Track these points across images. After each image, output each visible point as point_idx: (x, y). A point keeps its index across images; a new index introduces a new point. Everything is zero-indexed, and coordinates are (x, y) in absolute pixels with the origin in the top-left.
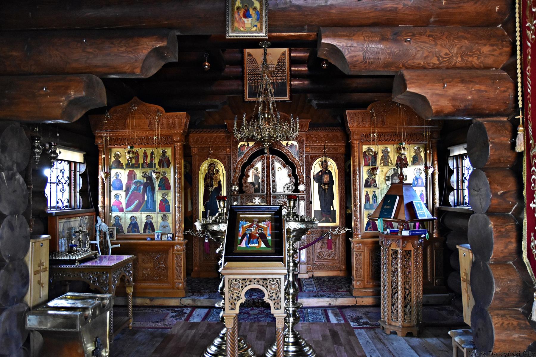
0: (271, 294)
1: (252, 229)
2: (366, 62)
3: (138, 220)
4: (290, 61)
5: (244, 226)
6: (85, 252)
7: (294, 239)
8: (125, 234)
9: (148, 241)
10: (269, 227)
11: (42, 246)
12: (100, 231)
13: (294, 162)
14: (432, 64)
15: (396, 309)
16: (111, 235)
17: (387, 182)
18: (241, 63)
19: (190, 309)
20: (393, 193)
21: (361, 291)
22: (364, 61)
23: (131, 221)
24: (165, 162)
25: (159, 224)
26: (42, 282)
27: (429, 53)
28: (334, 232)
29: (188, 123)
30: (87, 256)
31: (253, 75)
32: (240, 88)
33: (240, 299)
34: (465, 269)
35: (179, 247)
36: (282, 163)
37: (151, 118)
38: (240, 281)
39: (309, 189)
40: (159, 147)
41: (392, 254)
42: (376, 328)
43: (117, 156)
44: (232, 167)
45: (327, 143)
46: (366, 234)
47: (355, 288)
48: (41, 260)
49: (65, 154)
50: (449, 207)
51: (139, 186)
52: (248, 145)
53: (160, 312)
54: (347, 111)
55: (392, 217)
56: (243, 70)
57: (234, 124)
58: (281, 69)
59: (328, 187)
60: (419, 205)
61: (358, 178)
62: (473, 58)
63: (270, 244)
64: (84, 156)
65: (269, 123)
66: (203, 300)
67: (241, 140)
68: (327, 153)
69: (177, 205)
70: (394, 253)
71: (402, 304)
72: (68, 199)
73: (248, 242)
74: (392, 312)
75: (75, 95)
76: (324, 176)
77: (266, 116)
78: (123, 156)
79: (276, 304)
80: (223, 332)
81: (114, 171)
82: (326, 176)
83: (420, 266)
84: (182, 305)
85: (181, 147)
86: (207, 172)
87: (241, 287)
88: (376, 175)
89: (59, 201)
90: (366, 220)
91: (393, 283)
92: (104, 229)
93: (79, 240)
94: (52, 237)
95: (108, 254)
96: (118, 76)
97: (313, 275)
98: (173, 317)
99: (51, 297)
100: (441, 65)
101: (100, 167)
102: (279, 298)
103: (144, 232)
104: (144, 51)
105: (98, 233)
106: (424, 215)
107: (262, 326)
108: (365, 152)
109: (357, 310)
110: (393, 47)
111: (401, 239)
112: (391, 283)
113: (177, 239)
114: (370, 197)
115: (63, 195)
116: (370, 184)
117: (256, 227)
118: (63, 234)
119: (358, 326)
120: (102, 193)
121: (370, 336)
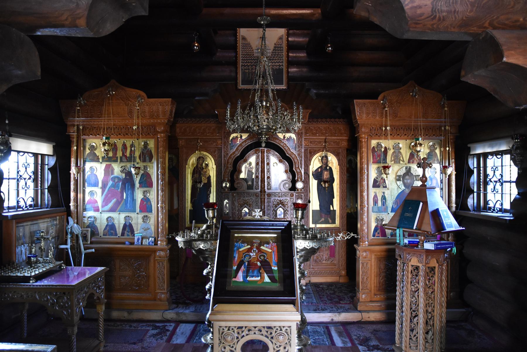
0: (277, 347)
1: (251, 254)
2: (436, 16)
3: (116, 222)
4: (287, 46)
5: (241, 250)
8: (100, 236)
9: (127, 246)
10: (274, 251)
12: (72, 233)
13: (291, 157)
15: (415, 336)
16: (85, 238)
17: (398, 182)
18: (234, 47)
19: (173, 325)
20: (415, 198)
21: (367, 305)
23: (108, 222)
24: (146, 156)
25: (139, 226)
29: (174, 111)
30: (47, 269)
32: (233, 74)
35: (162, 253)
36: (278, 158)
37: (131, 105)
38: (236, 330)
39: (307, 187)
41: (411, 271)
44: (223, 161)
46: (374, 240)
47: (360, 301)
51: (118, 182)
52: (241, 137)
53: (139, 328)
54: (355, 101)
55: (415, 228)
56: (237, 54)
57: (226, 113)
58: (278, 55)
59: (329, 185)
60: (445, 213)
61: (366, 177)
63: (276, 275)
64: (54, 147)
65: (267, 113)
66: (188, 313)
67: (234, 131)
68: (328, 148)
69: (159, 205)
72: (33, 197)
73: (247, 274)
74: (410, 339)
77: (264, 104)
82: (326, 173)
83: (443, 285)
84: (164, 319)
85: (165, 138)
86: (195, 166)
87: (236, 338)
88: (389, 174)
90: (373, 225)
91: (412, 305)
92: (76, 231)
93: (40, 248)
98: (154, 336)
103: (123, 234)
105: (69, 236)
106: (451, 227)
108: (374, 147)
109: (363, 327)
111: (424, 254)
112: (411, 304)
113: (160, 244)
115: (26, 192)
116: (379, 184)
117: (257, 251)
120: (74, 190)
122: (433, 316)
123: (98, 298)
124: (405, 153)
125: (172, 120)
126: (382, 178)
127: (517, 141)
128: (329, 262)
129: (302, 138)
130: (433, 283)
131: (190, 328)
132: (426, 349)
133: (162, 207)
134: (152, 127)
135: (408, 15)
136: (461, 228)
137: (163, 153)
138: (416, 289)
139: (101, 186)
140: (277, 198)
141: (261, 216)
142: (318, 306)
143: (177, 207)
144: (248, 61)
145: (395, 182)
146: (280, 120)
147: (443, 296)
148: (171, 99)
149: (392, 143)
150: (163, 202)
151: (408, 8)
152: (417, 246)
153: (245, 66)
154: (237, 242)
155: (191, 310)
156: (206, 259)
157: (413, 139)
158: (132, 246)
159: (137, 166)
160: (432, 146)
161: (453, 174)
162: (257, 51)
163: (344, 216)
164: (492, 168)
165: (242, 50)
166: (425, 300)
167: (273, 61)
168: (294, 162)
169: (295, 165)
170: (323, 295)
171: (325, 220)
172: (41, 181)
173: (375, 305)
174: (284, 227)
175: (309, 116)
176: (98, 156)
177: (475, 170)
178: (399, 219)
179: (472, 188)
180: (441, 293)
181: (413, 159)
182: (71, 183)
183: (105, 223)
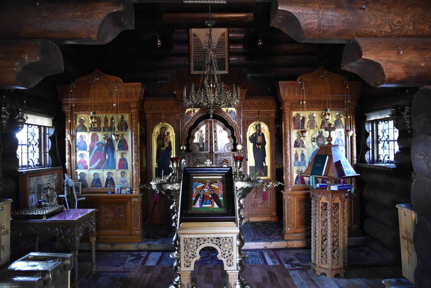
1: (205, 190)
2: (321, 29)
3: (101, 177)
4: (228, 41)
5: (198, 187)
6: (52, 206)
7: (241, 197)
8: (89, 188)
9: (110, 194)
10: (220, 188)
11: (2, 210)
12: (68, 186)
13: (233, 125)
14: (384, 33)
15: (325, 254)
16: (77, 189)
17: (313, 143)
18: (187, 42)
19: (146, 253)
20: (323, 153)
21: (292, 235)
22: (318, 29)
23: (94, 177)
24: (123, 126)
25: (118, 180)
26: (2, 245)
27: (382, 21)
28: (269, 185)
29: (143, 92)
30: (54, 210)
31: (198, 52)
32: (187, 63)
33: (194, 257)
34: (406, 228)
35: (137, 200)
36: (222, 126)
38: (195, 240)
39: (245, 148)
40: (118, 113)
41: (322, 207)
42: (307, 269)
43: (82, 121)
45: (260, 109)
47: (286, 233)
48: (1, 224)
49: (31, 119)
50: (366, 164)
51: (101, 146)
52: (194, 111)
53: (120, 256)
54: (279, 82)
55: (323, 174)
56: (189, 47)
60: (345, 164)
61: (289, 140)
62: (425, 26)
63: (222, 204)
66: (157, 245)
67: (190, 107)
68: (261, 118)
69: (133, 163)
70: (324, 206)
71: (331, 249)
72: (38, 158)
73: (202, 203)
74: (322, 256)
75: (29, 60)
76: (258, 138)
77: (212, 86)
78: (87, 121)
79: (229, 261)
80: (176, 280)
81: (79, 134)
82: (259, 137)
83: (345, 216)
85: (137, 113)
86: (159, 134)
87: (195, 246)
88: (305, 136)
89: (30, 161)
90: (295, 175)
91: (323, 231)
93: (47, 196)
94: (13, 200)
95: (74, 208)
96: (75, 42)
97: (248, 221)
98: (132, 261)
99: (13, 259)
100: (392, 34)
101: (67, 130)
102: (231, 256)
103: (106, 186)
104: (100, 16)
105: (66, 188)
107: (209, 268)
108: (294, 117)
109: (289, 252)
110: (347, 15)
112: (322, 231)
114: (299, 156)
116: (299, 144)
117: (209, 188)
118: (33, 190)
119: (292, 268)
120: (68, 153)
121: (303, 277)
122: (337, 239)
123: (92, 232)
124: (318, 121)
125: (142, 99)
126: (301, 140)
127: (393, 109)
128: (263, 206)
129: (240, 111)
130: (338, 215)
131: (159, 255)
132: (333, 263)
133: (135, 165)
134: (127, 104)
135: (303, 28)
136: (358, 175)
137: (135, 124)
138: (325, 220)
139: (89, 150)
140: (222, 157)
141: (210, 165)
142: (255, 237)
143: (146, 166)
144: (198, 53)
145: (311, 143)
146: (223, 98)
147: (345, 225)
148: (141, 83)
149: (308, 113)
150: (136, 161)
151: (303, 25)
152: (326, 189)
153: (196, 56)
154: (195, 182)
155: (159, 242)
156: (172, 197)
157: (323, 110)
158: (113, 195)
159: (116, 134)
160: (338, 115)
161: (354, 136)
162: (205, 45)
163: (274, 170)
164: (382, 131)
165: (193, 44)
166: (332, 227)
167: (217, 53)
168: (235, 129)
169: (236, 132)
170: (259, 230)
171: (259, 174)
172: (44, 147)
173: (298, 236)
174: (227, 172)
175: (245, 94)
176: (87, 127)
177: (370, 133)
178: (312, 168)
179: (368, 146)
180: (343, 222)
181: (324, 125)
182: (66, 148)
183: (92, 177)
